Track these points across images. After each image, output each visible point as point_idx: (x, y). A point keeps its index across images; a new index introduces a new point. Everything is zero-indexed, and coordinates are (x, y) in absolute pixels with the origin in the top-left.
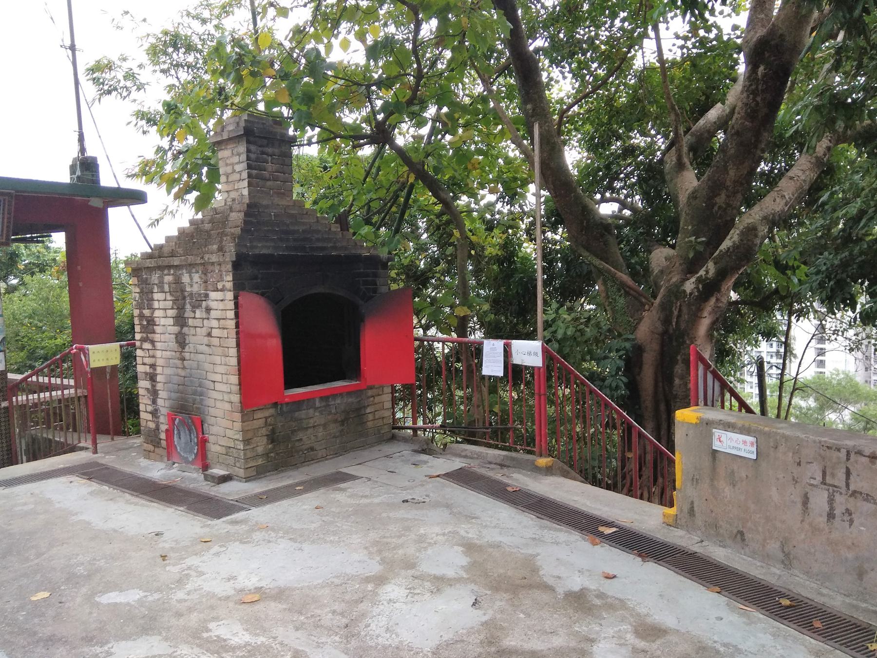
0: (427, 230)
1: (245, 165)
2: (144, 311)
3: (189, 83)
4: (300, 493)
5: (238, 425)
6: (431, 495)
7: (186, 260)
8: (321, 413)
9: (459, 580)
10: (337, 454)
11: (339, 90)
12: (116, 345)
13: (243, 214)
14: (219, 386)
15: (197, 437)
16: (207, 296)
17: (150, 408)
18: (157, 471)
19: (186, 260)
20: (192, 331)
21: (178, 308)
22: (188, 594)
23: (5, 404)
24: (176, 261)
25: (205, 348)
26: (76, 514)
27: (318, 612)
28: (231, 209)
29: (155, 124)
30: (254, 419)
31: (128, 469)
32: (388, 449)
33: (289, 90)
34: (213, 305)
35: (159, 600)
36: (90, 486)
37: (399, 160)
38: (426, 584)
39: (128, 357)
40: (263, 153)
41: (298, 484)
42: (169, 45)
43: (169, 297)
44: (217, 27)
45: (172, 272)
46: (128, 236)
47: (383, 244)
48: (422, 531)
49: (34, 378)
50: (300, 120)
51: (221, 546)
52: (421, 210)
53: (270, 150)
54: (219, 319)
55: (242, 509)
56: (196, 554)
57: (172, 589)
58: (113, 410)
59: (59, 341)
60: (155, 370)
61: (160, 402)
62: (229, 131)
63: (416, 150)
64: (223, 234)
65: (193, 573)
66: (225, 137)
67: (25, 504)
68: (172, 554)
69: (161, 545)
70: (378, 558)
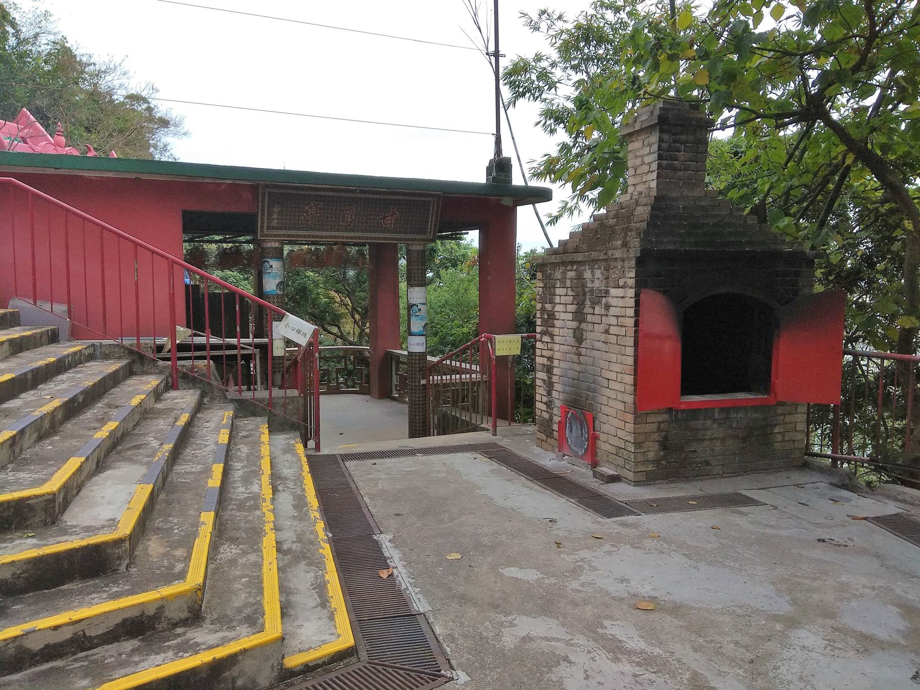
0: (859, 222)
1: (655, 156)
2: (546, 306)
3: (598, 76)
4: (693, 508)
5: (630, 427)
6: (856, 539)
7: (589, 256)
8: (720, 425)
9: (894, 645)
10: (736, 473)
11: (767, 64)
12: (518, 337)
13: (650, 208)
14: (613, 385)
15: (588, 433)
16: (607, 292)
17: (545, 399)
18: (549, 460)
19: (589, 256)
20: (590, 327)
22: (583, 585)
23: (423, 382)
24: (579, 257)
25: (606, 346)
26: (480, 488)
27: (719, 638)
28: (637, 203)
29: (563, 122)
30: (647, 423)
32: (797, 477)
33: (709, 71)
35: (555, 584)
36: (491, 465)
37: (835, 139)
38: (849, 639)
39: (528, 348)
40: (675, 141)
41: (693, 498)
42: (581, 41)
43: (570, 293)
44: (630, 14)
45: (575, 267)
46: (533, 232)
47: (806, 238)
48: (843, 578)
49: (448, 362)
50: (717, 102)
51: (612, 546)
52: (854, 198)
53: (683, 138)
54: (617, 317)
55: (632, 513)
56: (588, 548)
58: (512, 397)
59: (465, 330)
60: (552, 362)
61: (555, 394)
62: (642, 122)
63: (858, 126)
64: (626, 230)
65: (586, 566)
66: (637, 127)
67: (439, 472)
68: (565, 543)
69: (555, 532)
70: (788, 598)
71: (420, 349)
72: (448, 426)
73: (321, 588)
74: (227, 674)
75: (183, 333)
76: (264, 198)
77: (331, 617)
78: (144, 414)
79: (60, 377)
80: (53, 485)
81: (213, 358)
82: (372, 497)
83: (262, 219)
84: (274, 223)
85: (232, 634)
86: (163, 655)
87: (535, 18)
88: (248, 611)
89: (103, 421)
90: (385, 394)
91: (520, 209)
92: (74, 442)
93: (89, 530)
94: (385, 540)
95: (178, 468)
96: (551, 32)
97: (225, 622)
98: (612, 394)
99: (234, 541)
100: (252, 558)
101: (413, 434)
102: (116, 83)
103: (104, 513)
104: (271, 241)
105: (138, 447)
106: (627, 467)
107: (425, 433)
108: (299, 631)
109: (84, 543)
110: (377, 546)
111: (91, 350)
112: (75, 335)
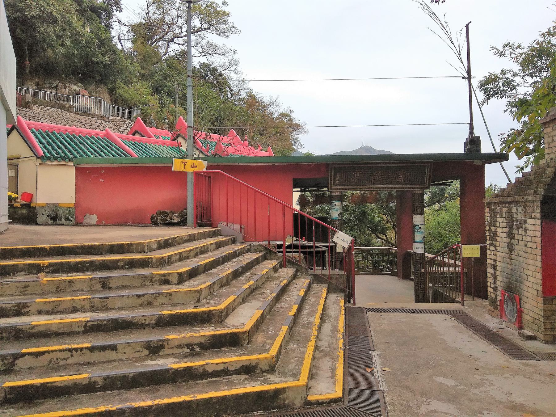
5: (541, 306)
7: (514, 199)
14: (530, 279)
16: (525, 221)
17: (493, 285)
18: (492, 323)
19: (514, 199)
21: (509, 228)
23: (423, 271)
24: (509, 199)
26: (441, 335)
30: (552, 304)
31: (477, 319)
34: (529, 227)
43: (505, 221)
45: (507, 205)
51: (511, 375)
55: (534, 359)
57: (472, 386)
58: (473, 281)
60: (496, 263)
61: (498, 283)
67: (419, 323)
69: (477, 363)
71: (421, 251)
72: (438, 298)
73: (333, 370)
74: (281, 396)
75: (290, 240)
76: (332, 170)
77: (335, 383)
78: (268, 278)
79: (234, 260)
80: (222, 306)
81: (304, 253)
82: (376, 332)
83: (331, 180)
84: (337, 182)
85: (285, 379)
86: (256, 383)
87: (501, 49)
88: (294, 372)
89: (248, 281)
90: (406, 277)
91: (487, 167)
92: (234, 289)
93: (234, 326)
94: (375, 355)
95: (278, 305)
96: (513, 56)
97: (284, 374)
98: (530, 285)
99: (296, 341)
100: (302, 350)
101: (417, 301)
102: (274, 110)
103: (241, 320)
104: (335, 192)
105: (262, 294)
106: (540, 330)
107: (426, 301)
108: (318, 386)
109: (231, 331)
110: (370, 357)
111: (249, 247)
112: (245, 239)
